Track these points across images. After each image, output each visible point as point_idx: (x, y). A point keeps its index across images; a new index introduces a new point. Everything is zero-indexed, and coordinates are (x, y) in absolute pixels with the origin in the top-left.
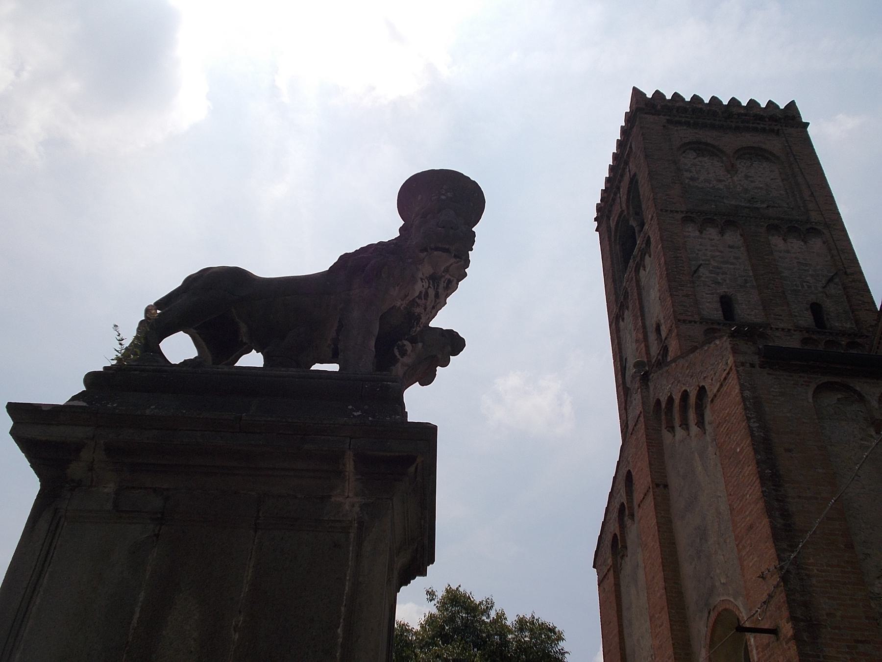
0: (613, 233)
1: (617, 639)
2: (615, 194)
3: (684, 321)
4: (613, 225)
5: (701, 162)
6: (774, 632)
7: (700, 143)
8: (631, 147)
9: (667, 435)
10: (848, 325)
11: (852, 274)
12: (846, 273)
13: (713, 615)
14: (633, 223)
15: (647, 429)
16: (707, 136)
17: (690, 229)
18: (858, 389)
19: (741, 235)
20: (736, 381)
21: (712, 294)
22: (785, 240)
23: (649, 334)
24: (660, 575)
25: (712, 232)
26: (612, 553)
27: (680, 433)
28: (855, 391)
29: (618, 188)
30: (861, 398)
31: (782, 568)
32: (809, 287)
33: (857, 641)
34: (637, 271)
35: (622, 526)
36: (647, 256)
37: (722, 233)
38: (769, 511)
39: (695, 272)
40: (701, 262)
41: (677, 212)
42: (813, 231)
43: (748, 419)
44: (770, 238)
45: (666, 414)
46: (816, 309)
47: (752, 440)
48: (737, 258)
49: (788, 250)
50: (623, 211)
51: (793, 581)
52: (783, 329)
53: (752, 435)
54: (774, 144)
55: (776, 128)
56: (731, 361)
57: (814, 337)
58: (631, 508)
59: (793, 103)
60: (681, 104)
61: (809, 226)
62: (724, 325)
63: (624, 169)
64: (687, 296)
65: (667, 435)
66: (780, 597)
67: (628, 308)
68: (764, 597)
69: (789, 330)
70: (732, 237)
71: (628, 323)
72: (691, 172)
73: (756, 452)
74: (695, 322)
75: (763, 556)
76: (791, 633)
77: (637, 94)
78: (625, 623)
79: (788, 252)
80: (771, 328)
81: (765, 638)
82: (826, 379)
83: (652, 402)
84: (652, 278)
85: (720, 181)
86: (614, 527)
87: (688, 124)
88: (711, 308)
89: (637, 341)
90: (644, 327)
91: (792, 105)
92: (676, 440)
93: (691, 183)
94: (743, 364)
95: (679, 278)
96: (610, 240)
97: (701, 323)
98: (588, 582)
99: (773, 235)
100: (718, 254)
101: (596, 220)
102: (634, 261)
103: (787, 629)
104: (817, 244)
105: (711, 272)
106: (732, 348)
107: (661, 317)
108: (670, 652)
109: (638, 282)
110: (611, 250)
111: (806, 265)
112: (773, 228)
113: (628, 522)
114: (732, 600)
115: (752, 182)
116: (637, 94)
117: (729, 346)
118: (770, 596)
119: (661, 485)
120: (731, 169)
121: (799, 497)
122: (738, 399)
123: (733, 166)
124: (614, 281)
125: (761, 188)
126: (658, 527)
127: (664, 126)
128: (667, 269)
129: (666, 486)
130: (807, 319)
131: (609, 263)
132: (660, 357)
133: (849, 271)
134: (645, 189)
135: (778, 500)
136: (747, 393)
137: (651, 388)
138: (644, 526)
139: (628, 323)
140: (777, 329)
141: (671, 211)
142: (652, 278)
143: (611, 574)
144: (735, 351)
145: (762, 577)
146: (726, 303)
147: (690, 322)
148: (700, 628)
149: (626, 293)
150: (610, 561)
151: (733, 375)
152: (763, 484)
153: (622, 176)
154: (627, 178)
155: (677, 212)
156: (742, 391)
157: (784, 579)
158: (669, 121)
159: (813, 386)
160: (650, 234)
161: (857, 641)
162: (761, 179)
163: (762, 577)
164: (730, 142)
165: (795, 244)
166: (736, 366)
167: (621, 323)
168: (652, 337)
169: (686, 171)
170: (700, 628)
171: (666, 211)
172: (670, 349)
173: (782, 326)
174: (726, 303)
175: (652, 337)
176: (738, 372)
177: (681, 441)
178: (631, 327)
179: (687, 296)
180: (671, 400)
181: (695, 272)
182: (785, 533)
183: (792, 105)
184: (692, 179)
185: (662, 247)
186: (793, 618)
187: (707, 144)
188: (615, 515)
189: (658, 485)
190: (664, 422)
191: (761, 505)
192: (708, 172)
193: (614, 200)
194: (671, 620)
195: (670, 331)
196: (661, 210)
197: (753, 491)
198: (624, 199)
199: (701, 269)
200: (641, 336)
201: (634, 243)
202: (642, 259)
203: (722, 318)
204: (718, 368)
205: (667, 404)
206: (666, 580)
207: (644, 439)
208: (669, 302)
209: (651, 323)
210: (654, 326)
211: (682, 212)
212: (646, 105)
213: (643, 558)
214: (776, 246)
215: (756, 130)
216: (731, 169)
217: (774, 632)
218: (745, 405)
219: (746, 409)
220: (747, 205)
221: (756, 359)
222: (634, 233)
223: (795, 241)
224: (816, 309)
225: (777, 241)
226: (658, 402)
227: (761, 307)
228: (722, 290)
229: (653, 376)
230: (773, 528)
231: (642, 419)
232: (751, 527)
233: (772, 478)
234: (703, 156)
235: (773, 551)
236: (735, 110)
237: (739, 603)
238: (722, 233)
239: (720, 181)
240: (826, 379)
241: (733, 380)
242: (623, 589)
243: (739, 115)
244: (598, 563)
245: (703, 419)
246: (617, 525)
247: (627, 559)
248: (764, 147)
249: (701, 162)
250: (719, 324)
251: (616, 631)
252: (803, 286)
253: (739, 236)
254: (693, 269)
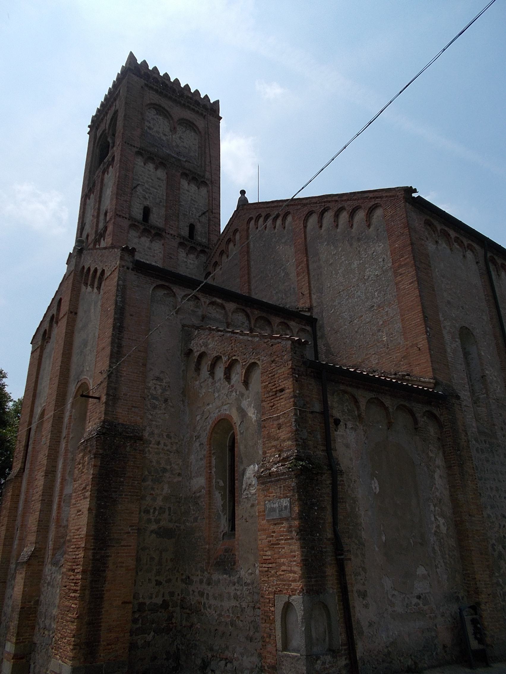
0: (97, 140)
1: (33, 385)
2: (104, 116)
3: (120, 216)
4: (98, 135)
5: (157, 118)
6: (99, 398)
7: (160, 106)
8: (119, 91)
9: (83, 287)
10: (204, 241)
11: (215, 213)
12: (212, 212)
13: (80, 383)
14: (109, 140)
15: (74, 280)
16: (165, 103)
17: (139, 160)
18: (174, 290)
19: (167, 173)
20: (117, 274)
21: (140, 204)
22: (189, 184)
23: (101, 214)
24: (60, 359)
25: (151, 166)
26: (42, 338)
27: (89, 289)
28: (173, 291)
29: (107, 113)
30: (175, 295)
31: (109, 371)
32: (192, 214)
33: (133, 407)
34: (103, 173)
35: (51, 326)
36: (111, 166)
37: (156, 169)
38: (113, 342)
39: (135, 188)
40: (140, 183)
41: (134, 146)
42: (204, 183)
43: (117, 296)
44: (181, 180)
45: (86, 276)
46: (192, 227)
47: (115, 307)
48: (159, 186)
49: (189, 190)
50: (105, 130)
51: (113, 378)
52: (171, 235)
53: (116, 304)
54: (200, 123)
55: (204, 114)
56: (118, 263)
57: (186, 243)
58: (57, 318)
59: (218, 101)
60: (156, 76)
61: (203, 180)
62: (142, 224)
63: (113, 103)
64: (126, 201)
65: (83, 287)
66: (105, 384)
67: (93, 193)
68: (99, 383)
69: (174, 236)
70: (161, 173)
71: (91, 202)
72: (150, 123)
73: (115, 313)
74: (126, 218)
75: (104, 364)
76: (104, 401)
77: (132, 58)
78: (40, 376)
79: (188, 191)
80: (166, 232)
81: (95, 401)
82: (160, 282)
83: (81, 266)
84: (110, 180)
85: (165, 135)
86: (46, 326)
87: (156, 91)
88: (137, 212)
89: (93, 216)
90: (99, 209)
91: (217, 103)
92: (86, 290)
93: (148, 130)
94: (123, 266)
95: (126, 188)
96: (94, 144)
97: (129, 219)
98: (26, 350)
99: (183, 179)
100: (151, 181)
101: (89, 126)
102: (103, 166)
103: (104, 399)
104: (204, 190)
105: (144, 191)
106: (121, 257)
107: (109, 208)
108: (54, 397)
109: (103, 179)
110: (93, 151)
111: (194, 201)
112: (185, 175)
113: (55, 325)
114: (88, 378)
115: (182, 142)
116: (132, 58)
117: (120, 255)
118: (102, 382)
119: (73, 312)
120: (173, 130)
121: (129, 339)
122: (116, 284)
123: (175, 128)
124: (90, 172)
125: (186, 148)
126: (66, 335)
127: (142, 87)
128: (118, 181)
129: (76, 313)
130: (185, 232)
131: (90, 159)
132: (102, 231)
133: (213, 211)
134: (120, 123)
135: (118, 339)
136: (121, 282)
137: (83, 258)
138: (59, 331)
139: (91, 202)
140: (168, 234)
141: (131, 145)
142: (110, 180)
143: (39, 350)
144: (122, 259)
145: (101, 373)
146: (147, 212)
147: (123, 217)
148: (73, 389)
149: (94, 183)
150: (40, 343)
151: (117, 270)
152: (113, 330)
153: (111, 106)
154: (113, 109)
155: (134, 146)
156: (118, 280)
157: (109, 376)
158: (146, 85)
159: (154, 285)
160: (116, 154)
161: (133, 407)
162: (187, 141)
163: (101, 373)
164: (178, 112)
165: (193, 188)
166: (120, 267)
167: (88, 200)
168: (102, 217)
169: (147, 121)
170: (73, 389)
171: (128, 144)
172: (108, 229)
173: (172, 232)
174: (147, 212)
175: (102, 217)
176: (119, 270)
177: (88, 293)
178: (92, 204)
179: (126, 201)
180: (89, 269)
181: (135, 188)
182: (117, 353)
183: (217, 103)
184: (149, 128)
185: (119, 166)
186: (107, 394)
187: (164, 108)
188: (48, 319)
189: (71, 312)
190: (83, 280)
191: (110, 339)
192: (159, 126)
193: (102, 119)
194: (59, 383)
195: (111, 218)
196: (125, 142)
197: (109, 332)
198: (108, 122)
199: (139, 188)
200: (96, 214)
201: (108, 153)
202: (108, 167)
203: (141, 219)
204: (111, 264)
205: (87, 270)
206: (62, 362)
207: (71, 285)
208: (114, 202)
209: (103, 208)
210: (104, 211)
211: (137, 148)
212: (135, 67)
213: (56, 346)
214: (183, 186)
215: (193, 110)
216: (173, 130)
217: (99, 398)
218: (117, 288)
219: (117, 290)
220: (175, 156)
221: (131, 265)
222: (109, 146)
223: (193, 186)
224: (192, 227)
225: (184, 183)
226: (83, 267)
227: (164, 219)
228: (147, 203)
229: (85, 252)
230: (112, 352)
231: (73, 273)
232: (104, 349)
233: (119, 328)
234: (160, 115)
235: (108, 362)
236: (186, 93)
237: (91, 381)
238: (156, 169)
239: (165, 135)
240: (160, 282)
241: (116, 274)
242: (43, 360)
243: (188, 97)
244: (34, 342)
245: (101, 286)
246: (48, 325)
247: (49, 344)
248: (195, 122)
249: (157, 118)
250: (138, 222)
251: (34, 380)
252: (189, 213)
253: (165, 174)
254: (134, 185)
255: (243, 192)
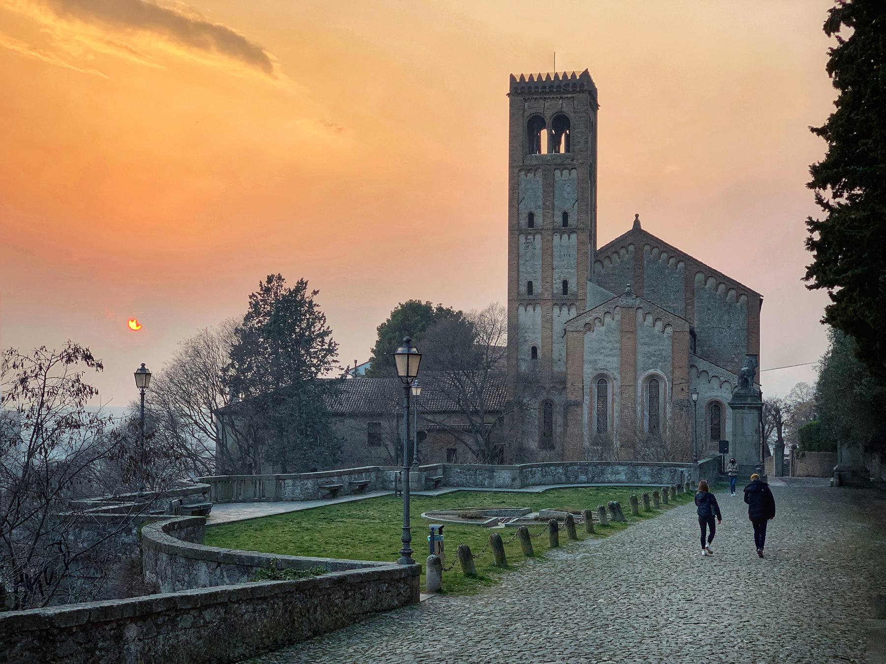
255: (637, 216)
